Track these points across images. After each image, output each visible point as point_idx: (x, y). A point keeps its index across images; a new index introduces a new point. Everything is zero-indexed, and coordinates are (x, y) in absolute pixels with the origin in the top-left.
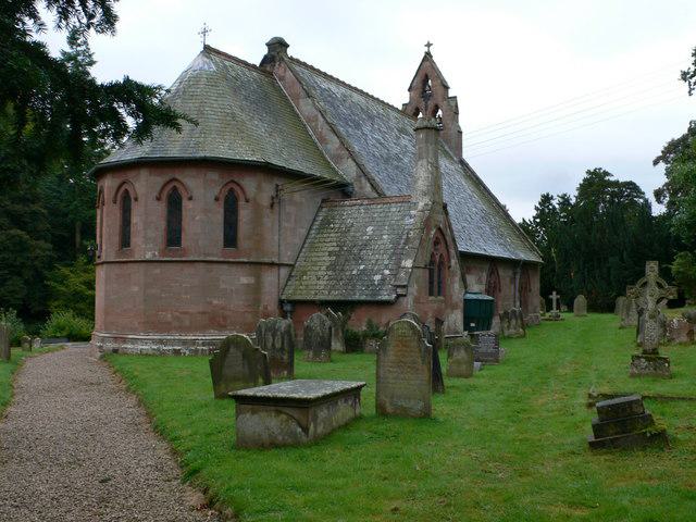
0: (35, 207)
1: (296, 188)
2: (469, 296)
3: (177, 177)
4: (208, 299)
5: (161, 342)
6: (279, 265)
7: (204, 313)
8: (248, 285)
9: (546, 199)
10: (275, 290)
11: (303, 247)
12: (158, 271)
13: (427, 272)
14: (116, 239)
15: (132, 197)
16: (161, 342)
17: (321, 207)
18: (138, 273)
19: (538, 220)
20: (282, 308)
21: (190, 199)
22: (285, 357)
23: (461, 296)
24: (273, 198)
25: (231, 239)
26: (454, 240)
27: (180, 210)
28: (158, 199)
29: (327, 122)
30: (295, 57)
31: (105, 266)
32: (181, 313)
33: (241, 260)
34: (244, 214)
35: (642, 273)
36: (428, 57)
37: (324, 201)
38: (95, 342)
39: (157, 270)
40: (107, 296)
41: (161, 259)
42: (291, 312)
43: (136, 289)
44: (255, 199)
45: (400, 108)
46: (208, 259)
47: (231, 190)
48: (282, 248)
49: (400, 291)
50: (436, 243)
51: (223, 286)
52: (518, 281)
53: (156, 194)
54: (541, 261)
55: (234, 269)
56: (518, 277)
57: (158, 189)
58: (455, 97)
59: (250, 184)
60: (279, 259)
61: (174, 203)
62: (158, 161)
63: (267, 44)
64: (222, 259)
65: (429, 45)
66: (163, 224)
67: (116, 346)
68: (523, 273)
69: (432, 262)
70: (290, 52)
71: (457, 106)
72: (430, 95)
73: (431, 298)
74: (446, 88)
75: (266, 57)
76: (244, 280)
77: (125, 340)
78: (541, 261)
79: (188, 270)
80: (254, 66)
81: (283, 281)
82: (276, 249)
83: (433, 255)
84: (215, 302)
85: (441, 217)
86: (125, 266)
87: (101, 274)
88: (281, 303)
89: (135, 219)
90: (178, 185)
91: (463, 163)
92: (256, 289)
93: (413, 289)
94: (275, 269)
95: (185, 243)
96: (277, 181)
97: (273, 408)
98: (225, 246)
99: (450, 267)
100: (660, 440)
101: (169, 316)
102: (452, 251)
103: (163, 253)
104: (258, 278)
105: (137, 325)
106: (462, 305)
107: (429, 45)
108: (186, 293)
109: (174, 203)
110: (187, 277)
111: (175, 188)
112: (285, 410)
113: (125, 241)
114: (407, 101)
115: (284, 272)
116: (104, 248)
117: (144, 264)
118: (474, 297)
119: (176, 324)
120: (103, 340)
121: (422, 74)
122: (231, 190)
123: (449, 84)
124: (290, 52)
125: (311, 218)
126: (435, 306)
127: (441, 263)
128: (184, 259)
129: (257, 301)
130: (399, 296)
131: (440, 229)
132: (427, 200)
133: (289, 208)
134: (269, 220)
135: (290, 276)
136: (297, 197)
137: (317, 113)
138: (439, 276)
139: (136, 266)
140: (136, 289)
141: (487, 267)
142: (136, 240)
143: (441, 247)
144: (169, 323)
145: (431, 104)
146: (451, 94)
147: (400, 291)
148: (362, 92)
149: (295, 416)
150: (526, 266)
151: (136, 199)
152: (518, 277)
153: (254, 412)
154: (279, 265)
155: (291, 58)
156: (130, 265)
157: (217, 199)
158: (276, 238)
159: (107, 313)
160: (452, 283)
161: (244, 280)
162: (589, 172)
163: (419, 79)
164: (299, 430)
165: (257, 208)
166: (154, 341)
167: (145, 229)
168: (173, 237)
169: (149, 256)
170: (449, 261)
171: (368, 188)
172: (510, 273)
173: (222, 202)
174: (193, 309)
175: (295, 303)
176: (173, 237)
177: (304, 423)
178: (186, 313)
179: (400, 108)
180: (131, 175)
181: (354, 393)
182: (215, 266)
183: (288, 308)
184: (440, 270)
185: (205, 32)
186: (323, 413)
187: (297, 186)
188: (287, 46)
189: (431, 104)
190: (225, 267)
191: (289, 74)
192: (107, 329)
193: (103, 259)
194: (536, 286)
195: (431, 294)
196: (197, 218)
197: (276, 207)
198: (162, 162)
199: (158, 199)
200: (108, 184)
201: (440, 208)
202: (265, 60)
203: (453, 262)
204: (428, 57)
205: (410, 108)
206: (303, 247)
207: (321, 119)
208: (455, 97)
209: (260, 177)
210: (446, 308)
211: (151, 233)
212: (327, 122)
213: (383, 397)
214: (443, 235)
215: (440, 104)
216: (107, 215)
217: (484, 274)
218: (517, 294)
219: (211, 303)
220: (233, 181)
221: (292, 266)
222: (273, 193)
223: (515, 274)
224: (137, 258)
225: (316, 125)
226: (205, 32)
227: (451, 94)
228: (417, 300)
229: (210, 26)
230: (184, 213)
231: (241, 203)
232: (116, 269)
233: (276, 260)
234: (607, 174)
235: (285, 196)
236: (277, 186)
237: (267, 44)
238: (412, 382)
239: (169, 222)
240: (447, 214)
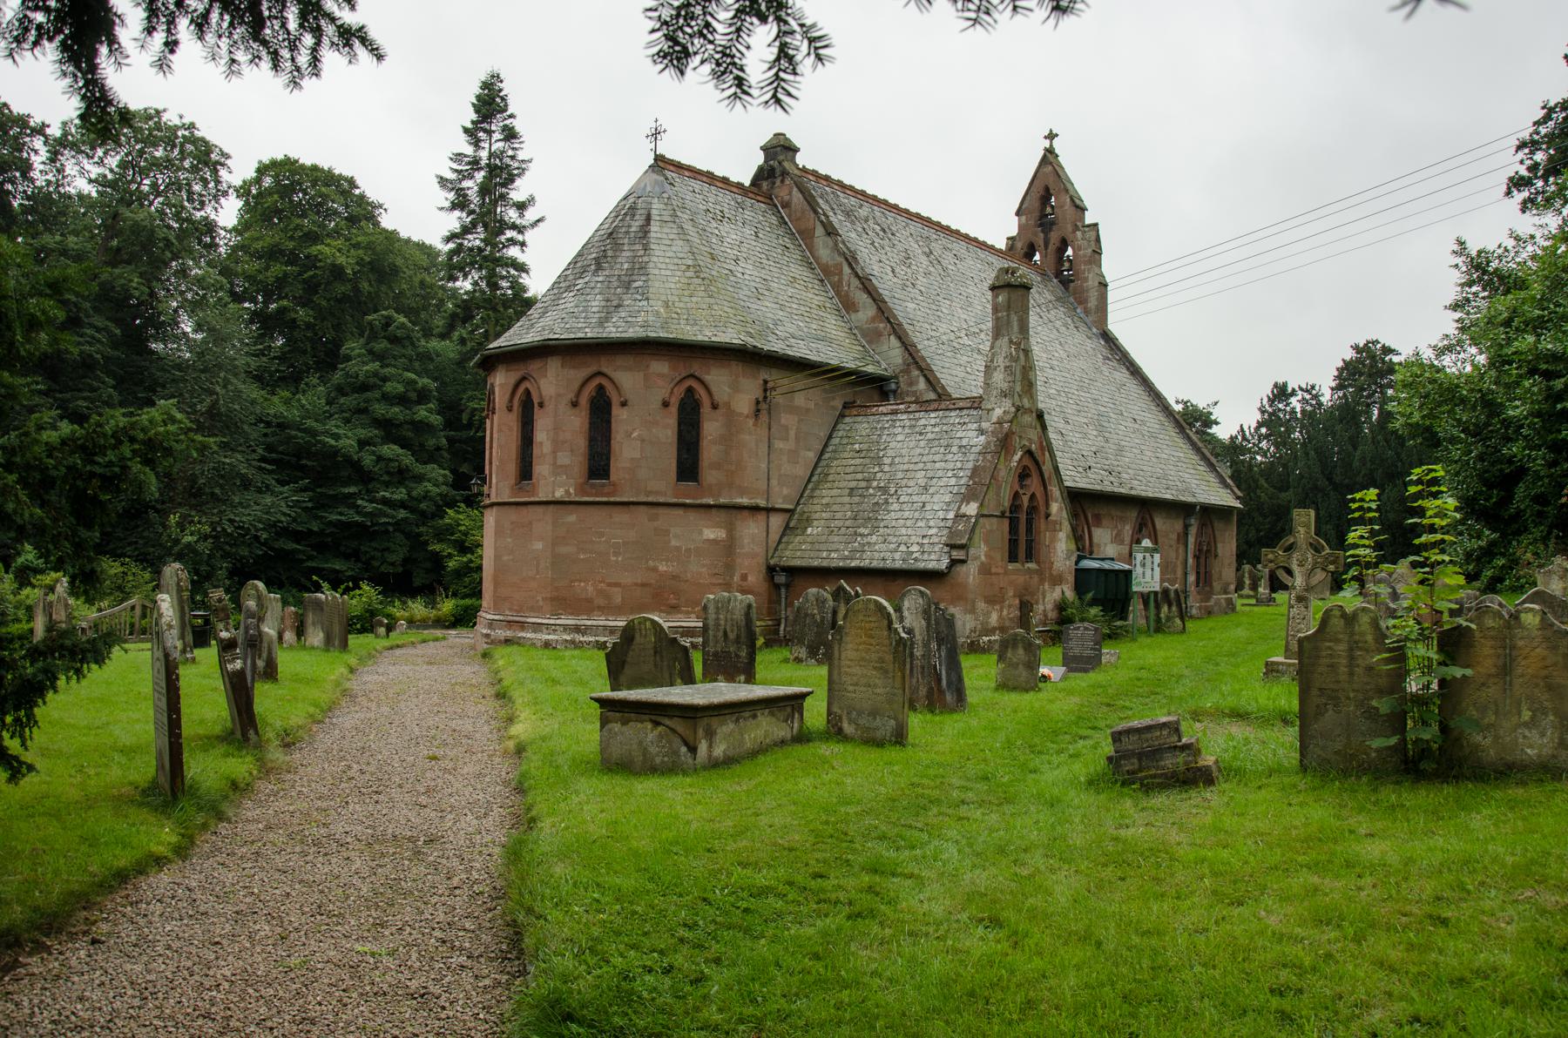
0: (422, 413)
1: (800, 385)
2: (1088, 564)
3: (605, 370)
4: (651, 563)
5: (577, 629)
6: (769, 510)
7: (643, 585)
8: (715, 542)
9: (1281, 392)
10: (760, 550)
11: (809, 481)
12: (572, 518)
13: (1006, 522)
14: (512, 468)
15: (536, 401)
16: (577, 629)
17: (842, 416)
18: (543, 521)
19: (1263, 430)
20: (772, 578)
21: (624, 404)
22: (743, 654)
23: (1071, 563)
24: (758, 402)
25: (688, 469)
26: (1057, 469)
27: (609, 422)
28: (575, 404)
29: (857, 275)
30: (810, 167)
31: (495, 509)
32: (609, 585)
33: (704, 501)
34: (711, 428)
35: (1287, 529)
36: (1049, 157)
37: (846, 406)
38: (482, 629)
39: (572, 517)
40: (497, 557)
41: (577, 499)
42: (787, 586)
43: (539, 546)
44: (728, 405)
45: (1003, 247)
46: (650, 499)
47: (690, 390)
48: (774, 482)
49: (956, 554)
50: (1023, 475)
51: (674, 543)
52: (1191, 540)
53: (571, 396)
54: (1238, 505)
55: (692, 516)
56: (1193, 531)
57: (576, 385)
58: (1096, 225)
59: (719, 379)
60: (768, 500)
61: (600, 411)
62: (510, 352)
63: (761, 148)
64: (674, 500)
65: (1051, 136)
66: (582, 443)
67: (509, 634)
68: (1202, 526)
69: (1015, 507)
70: (801, 160)
71: (1098, 240)
72: (1053, 223)
73: (1011, 566)
74: (1083, 209)
75: (761, 169)
76: (710, 533)
77: (522, 626)
78: (1238, 505)
79: (621, 516)
80: (739, 186)
81: (774, 537)
82: (763, 485)
83: (1016, 496)
84: (662, 568)
85: (1033, 434)
86: (524, 510)
87: (490, 518)
88: (771, 570)
89: (541, 436)
90: (604, 382)
91: (1109, 339)
92: (729, 548)
93: (980, 551)
94: (762, 517)
95: (613, 477)
96: (764, 374)
97: (647, 717)
98: (678, 480)
99: (1048, 516)
100: (1196, 777)
101: (590, 588)
102: (1055, 491)
103: (581, 489)
104: (731, 530)
105: (541, 603)
106: (1071, 578)
107: (1051, 136)
108: (616, 554)
109: (600, 411)
110: (617, 530)
111: (601, 388)
112: (667, 721)
113: (525, 472)
114: (1014, 232)
115: (777, 521)
116: (494, 481)
117: (551, 508)
118: (1106, 565)
119: (600, 601)
120: (491, 624)
121: (1039, 185)
122: (690, 390)
123: (1087, 203)
124: (801, 160)
125: (823, 434)
126: (1021, 579)
127: (1033, 509)
128: (612, 499)
129: (730, 567)
130: (954, 562)
131: (1029, 453)
132: (1007, 405)
133: (786, 419)
134: (751, 437)
135: (787, 527)
136: (800, 400)
137: (841, 259)
138: (1029, 530)
139: (540, 509)
140: (539, 546)
141: (1133, 514)
142: (541, 469)
143: (1034, 484)
144: (589, 601)
145: (1054, 237)
146: (1089, 219)
147: (956, 554)
148: (928, 220)
149: (680, 729)
150: (1209, 513)
151: (541, 405)
152: (1193, 531)
153: (625, 723)
154: (769, 510)
155: (804, 170)
156: (531, 509)
157: (666, 404)
158: (764, 466)
159: (497, 583)
160: (1054, 540)
161: (710, 533)
162: (1356, 348)
163: (1035, 195)
164: (684, 749)
165: (731, 414)
166: (566, 628)
167: (554, 452)
168: (598, 465)
169: (559, 494)
170: (1047, 505)
171: (922, 384)
172: (1178, 525)
173: (674, 409)
174: (627, 579)
175: (793, 572)
176: (598, 465)
177: (690, 739)
178: (617, 585)
179: (1003, 247)
180: (534, 367)
181: (795, 702)
182: (661, 511)
183: (781, 579)
184: (1029, 522)
185: (656, 134)
186: (726, 729)
187: (799, 381)
188: (795, 150)
189: (1054, 237)
190: (680, 512)
191: (797, 196)
192: (497, 608)
193: (494, 499)
194: (1227, 546)
195: (1013, 557)
196: (635, 434)
197: (764, 417)
198: (598, 345)
199: (575, 404)
200: (501, 381)
201: (1028, 419)
202: (763, 175)
203: (1055, 507)
204: (1049, 157)
205: (1019, 245)
206: (809, 481)
207: (846, 270)
208: (1096, 225)
209: (737, 367)
210: (1042, 581)
211: (564, 458)
212: (857, 275)
213: (835, 709)
214: (1037, 463)
215: (1070, 238)
216: (500, 431)
217: (1128, 527)
218: (1190, 561)
219: (655, 569)
220: (692, 376)
221: (791, 512)
222: (759, 394)
223: (1186, 527)
224: (542, 497)
225: (840, 281)
226: (656, 134)
227: (1089, 219)
228: (985, 570)
229: (664, 123)
230: (614, 425)
231: (706, 409)
232: (512, 515)
233: (762, 503)
234: (1387, 350)
235: (778, 398)
236: (766, 382)
237: (761, 148)
238: (878, 691)
239: (592, 440)
240: (1044, 427)
